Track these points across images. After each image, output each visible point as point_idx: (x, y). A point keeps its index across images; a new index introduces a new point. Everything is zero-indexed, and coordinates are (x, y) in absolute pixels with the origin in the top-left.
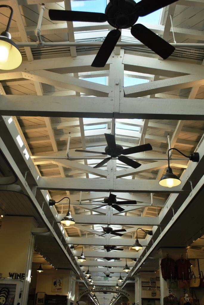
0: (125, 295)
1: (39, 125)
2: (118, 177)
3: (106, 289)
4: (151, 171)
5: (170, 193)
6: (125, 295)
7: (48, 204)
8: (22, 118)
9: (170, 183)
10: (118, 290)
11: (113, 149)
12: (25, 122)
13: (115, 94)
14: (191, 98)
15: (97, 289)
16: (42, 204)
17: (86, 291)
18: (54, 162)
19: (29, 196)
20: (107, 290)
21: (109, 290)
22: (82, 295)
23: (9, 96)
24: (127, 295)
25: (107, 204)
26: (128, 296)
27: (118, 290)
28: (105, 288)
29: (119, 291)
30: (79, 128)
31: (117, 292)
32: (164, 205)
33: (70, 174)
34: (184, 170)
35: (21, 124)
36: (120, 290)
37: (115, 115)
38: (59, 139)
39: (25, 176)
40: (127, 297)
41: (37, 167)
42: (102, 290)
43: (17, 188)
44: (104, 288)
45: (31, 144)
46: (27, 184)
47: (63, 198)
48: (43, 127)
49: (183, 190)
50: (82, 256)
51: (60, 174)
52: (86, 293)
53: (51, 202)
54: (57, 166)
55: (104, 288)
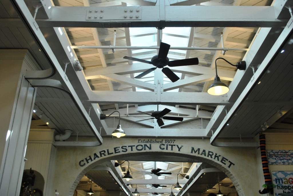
0: (221, 164)
1: (85, 38)
2: (165, 90)
3: (160, 148)
4: (196, 84)
5: (217, 106)
6: (221, 164)
7: (99, 117)
8: (72, 29)
9: (218, 92)
10: (199, 149)
11: (161, 58)
12: (74, 35)
13: (159, 90)
14: (203, 92)
15: (132, 147)
16: (65, 65)
17: (99, 155)
18: (102, 77)
19: (71, 92)
20: (165, 151)
21: (169, 150)
22: (87, 165)
23: (93, 91)
24: (228, 164)
25: (154, 118)
26: (229, 167)
27: (199, 149)
28: (158, 145)
29: (201, 151)
30: (125, 40)
31: (194, 154)
32: (211, 116)
33: (119, 89)
34: (215, 108)
35: (69, 34)
36: (204, 151)
37: (161, 25)
38: (104, 40)
39: (66, 69)
40: (228, 169)
41: (87, 81)
42: (147, 150)
43: (56, 83)
44: (153, 145)
45: (81, 58)
46: (91, 119)
47: (114, 111)
48: (106, 82)
49: (228, 103)
50: (119, 128)
51: (93, 39)
52: (97, 159)
53: (102, 116)
54: (105, 80)
55: (153, 145)
